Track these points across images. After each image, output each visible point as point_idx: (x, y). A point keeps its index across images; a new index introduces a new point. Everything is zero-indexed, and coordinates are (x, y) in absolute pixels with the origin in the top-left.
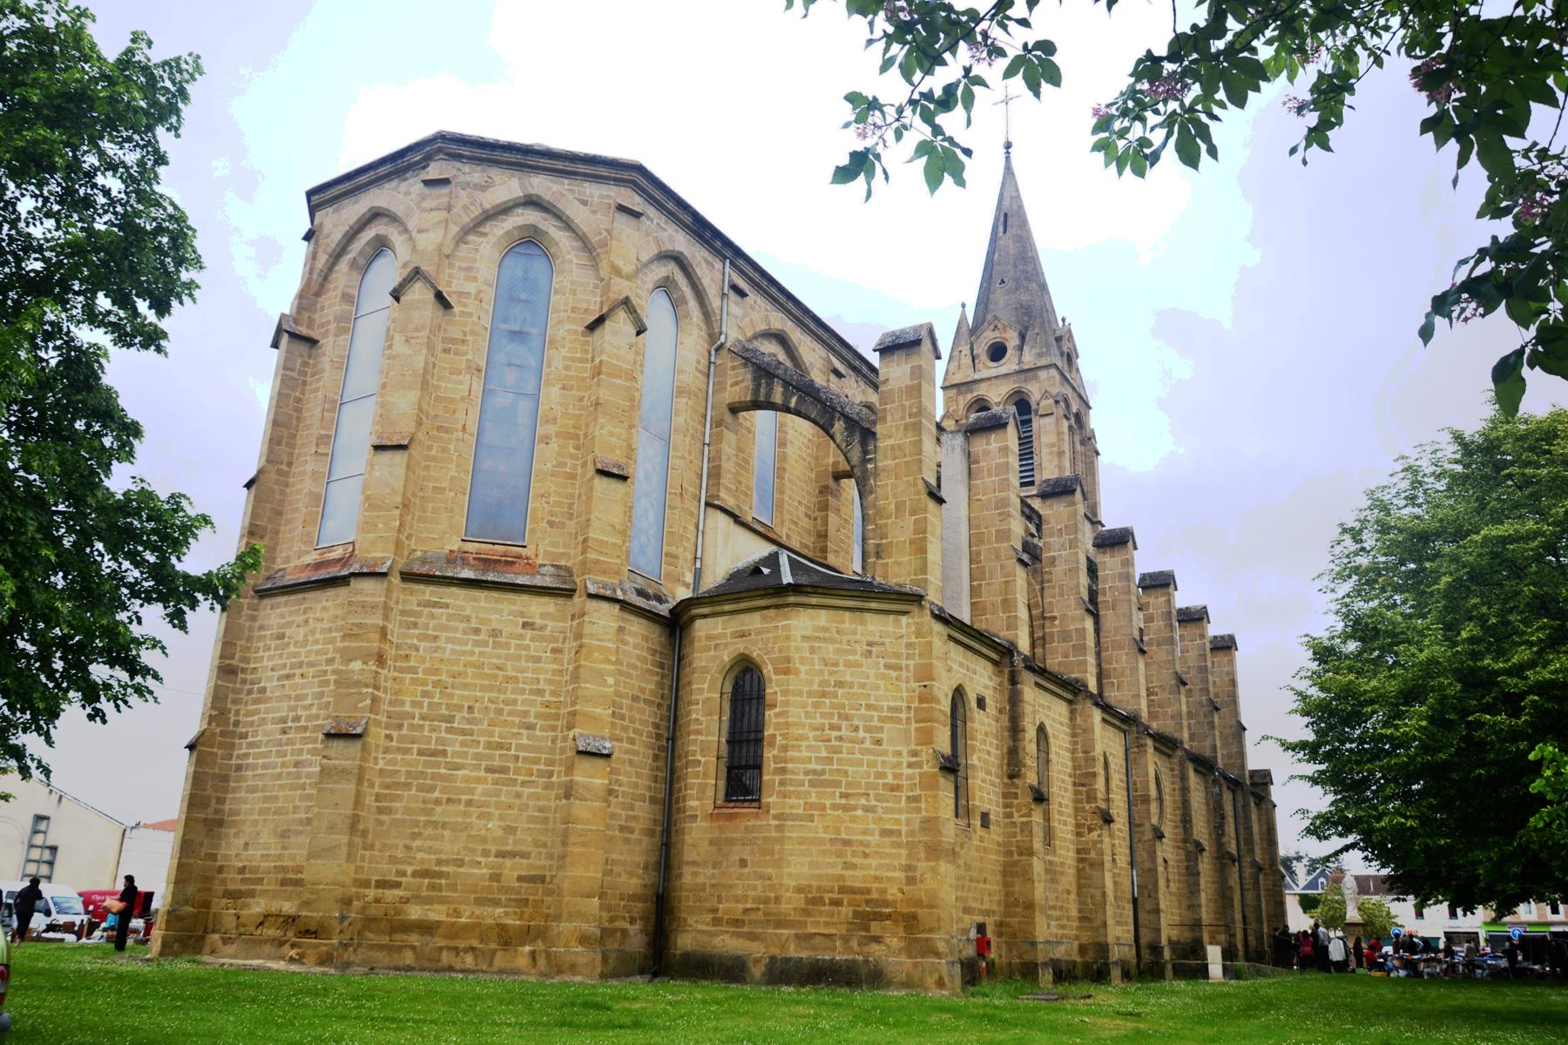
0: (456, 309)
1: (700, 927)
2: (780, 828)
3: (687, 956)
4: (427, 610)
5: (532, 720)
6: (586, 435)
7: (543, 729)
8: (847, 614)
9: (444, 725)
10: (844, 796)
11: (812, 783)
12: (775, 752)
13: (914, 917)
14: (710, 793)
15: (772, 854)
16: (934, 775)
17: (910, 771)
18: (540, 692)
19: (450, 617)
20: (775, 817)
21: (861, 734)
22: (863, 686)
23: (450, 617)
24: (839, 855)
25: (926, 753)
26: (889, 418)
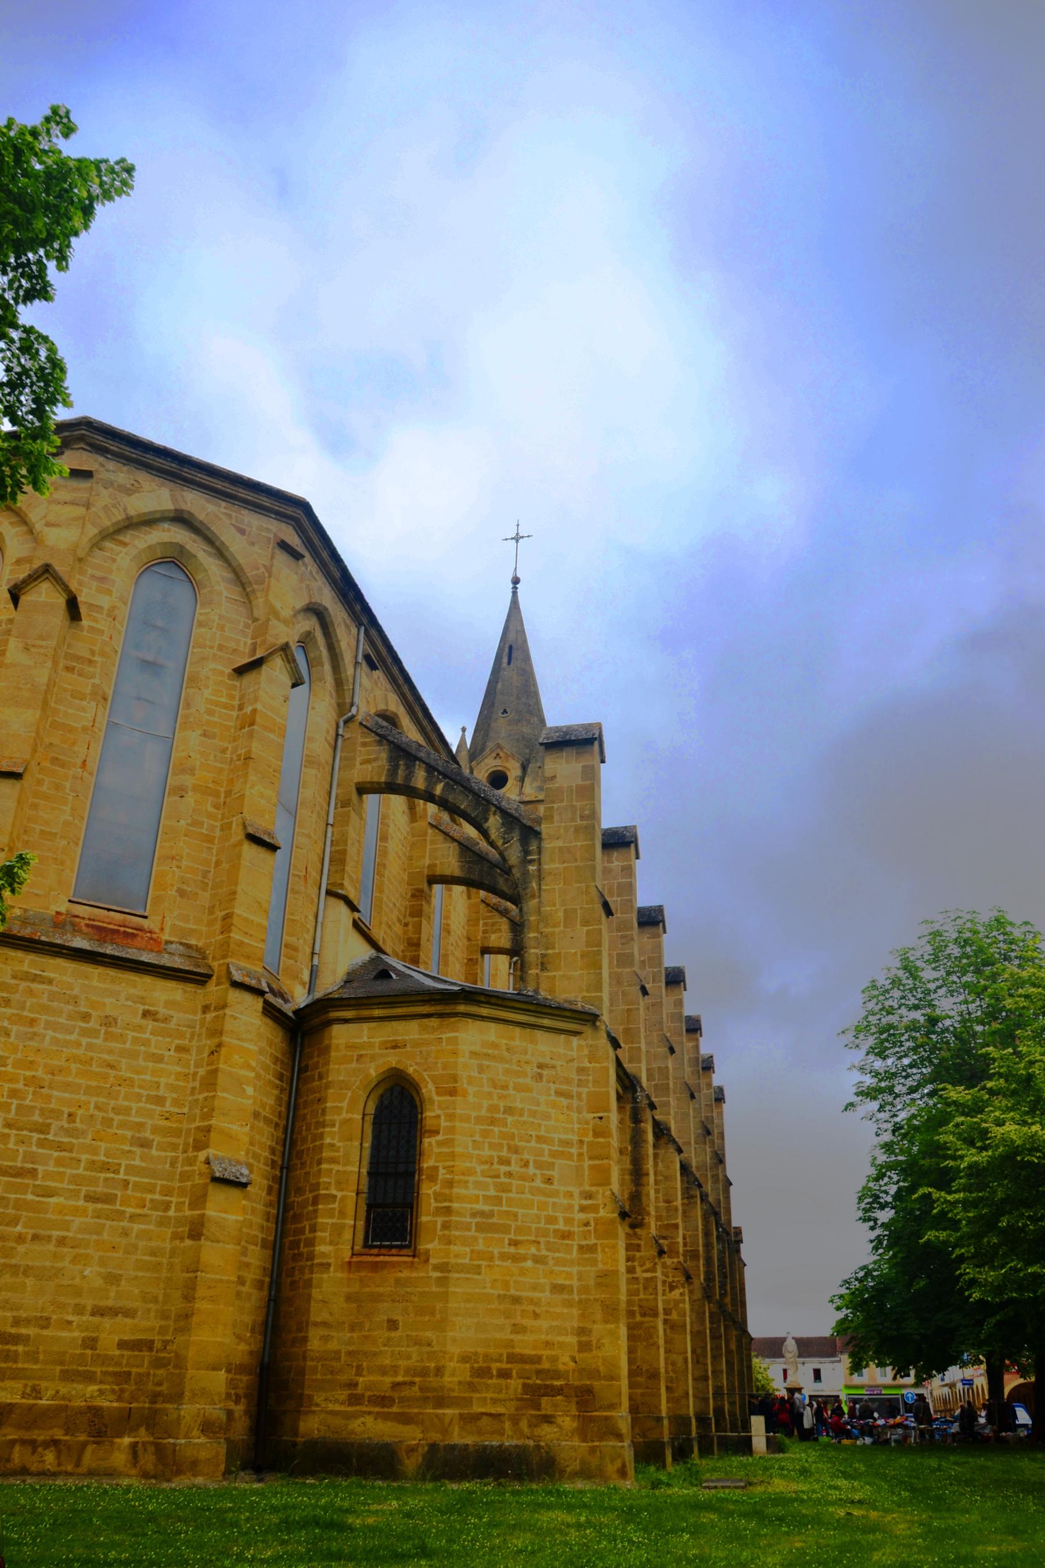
0: (85, 622)
1: (331, 1407)
2: (443, 1281)
3: (313, 1445)
4: (23, 985)
5: (148, 1135)
6: (228, 793)
7: (161, 1148)
8: (518, 1030)
9: (35, 1136)
10: (514, 1243)
11: (480, 1228)
12: (437, 1188)
13: (589, 1391)
14: (348, 1235)
15: (433, 1314)
16: (612, 1221)
17: (583, 1216)
18: (160, 1100)
19: (53, 996)
20: (436, 1268)
21: (531, 1170)
22: (533, 1114)
23: (53, 996)
24: (507, 1315)
25: (602, 1195)
26: (556, 818)
